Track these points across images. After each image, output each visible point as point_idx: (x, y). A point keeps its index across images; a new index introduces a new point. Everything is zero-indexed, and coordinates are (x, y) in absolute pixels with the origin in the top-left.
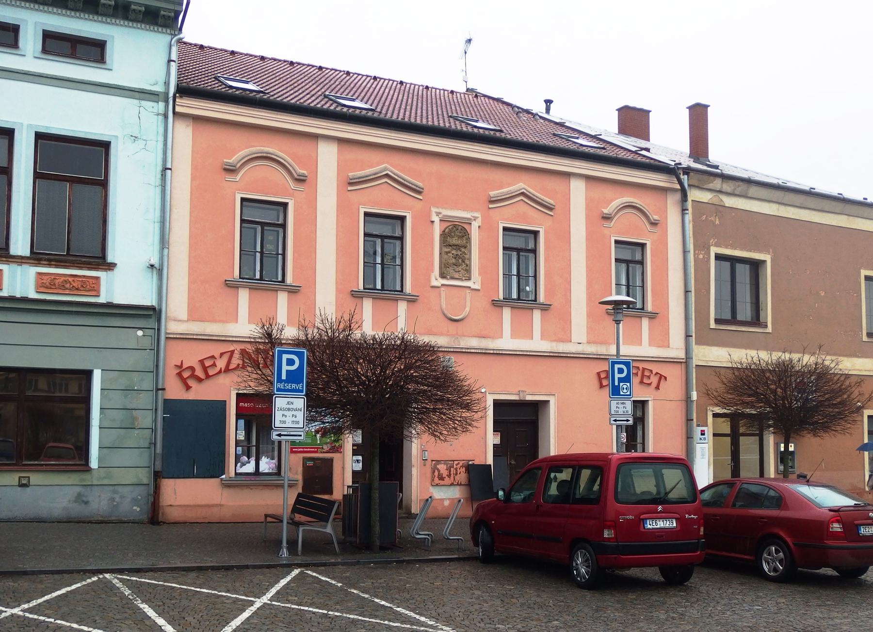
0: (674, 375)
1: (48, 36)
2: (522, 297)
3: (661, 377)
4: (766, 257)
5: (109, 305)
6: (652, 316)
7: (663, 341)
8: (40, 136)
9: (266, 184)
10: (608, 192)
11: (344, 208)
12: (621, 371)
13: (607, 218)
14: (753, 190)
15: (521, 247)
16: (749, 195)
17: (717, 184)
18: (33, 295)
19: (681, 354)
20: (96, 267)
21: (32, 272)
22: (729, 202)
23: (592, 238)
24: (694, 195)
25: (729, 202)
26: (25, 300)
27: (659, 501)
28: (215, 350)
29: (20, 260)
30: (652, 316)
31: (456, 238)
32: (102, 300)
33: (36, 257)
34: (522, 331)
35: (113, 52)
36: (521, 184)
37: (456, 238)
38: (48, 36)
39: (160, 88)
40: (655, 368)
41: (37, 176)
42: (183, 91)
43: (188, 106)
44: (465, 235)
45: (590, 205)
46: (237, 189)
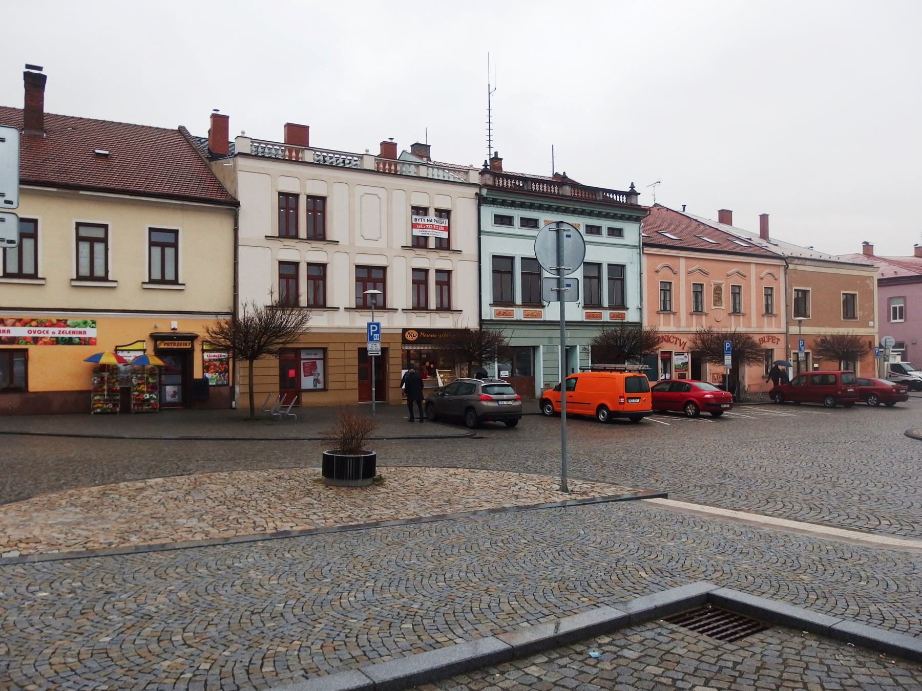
0: (782, 338)
1: (522, 219)
2: (736, 311)
3: (779, 340)
4: (810, 289)
5: (544, 321)
6: (675, 314)
7: (779, 326)
8: (495, 257)
9: (665, 275)
10: (656, 259)
11: (687, 282)
12: (374, 328)
13: (762, 279)
14: (808, 263)
15: (736, 292)
16: (482, 237)
17: (796, 261)
18: (523, 319)
19: (784, 330)
20: (512, 306)
21: (522, 310)
22: (799, 268)
23: (757, 287)
24: (791, 267)
25: (799, 268)
26: (491, 320)
27: (849, 384)
28: (762, 336)
29: (519, 306)
30: (675, 314)
31: (718, 290)
32: (514, 319)
33: (610, 308)
34: (667, 324)
35: (626, 233)
36: (735, 268)
37: (718, 290)
38: (522, 219)
39: (637, 244)
40: (777, 336)
41: (522, 273)
42: (646, 245)
43: (648, 250)
44: (720, 289)
45: (757, 274)
46: (660, 278)
